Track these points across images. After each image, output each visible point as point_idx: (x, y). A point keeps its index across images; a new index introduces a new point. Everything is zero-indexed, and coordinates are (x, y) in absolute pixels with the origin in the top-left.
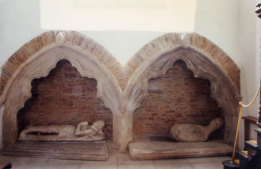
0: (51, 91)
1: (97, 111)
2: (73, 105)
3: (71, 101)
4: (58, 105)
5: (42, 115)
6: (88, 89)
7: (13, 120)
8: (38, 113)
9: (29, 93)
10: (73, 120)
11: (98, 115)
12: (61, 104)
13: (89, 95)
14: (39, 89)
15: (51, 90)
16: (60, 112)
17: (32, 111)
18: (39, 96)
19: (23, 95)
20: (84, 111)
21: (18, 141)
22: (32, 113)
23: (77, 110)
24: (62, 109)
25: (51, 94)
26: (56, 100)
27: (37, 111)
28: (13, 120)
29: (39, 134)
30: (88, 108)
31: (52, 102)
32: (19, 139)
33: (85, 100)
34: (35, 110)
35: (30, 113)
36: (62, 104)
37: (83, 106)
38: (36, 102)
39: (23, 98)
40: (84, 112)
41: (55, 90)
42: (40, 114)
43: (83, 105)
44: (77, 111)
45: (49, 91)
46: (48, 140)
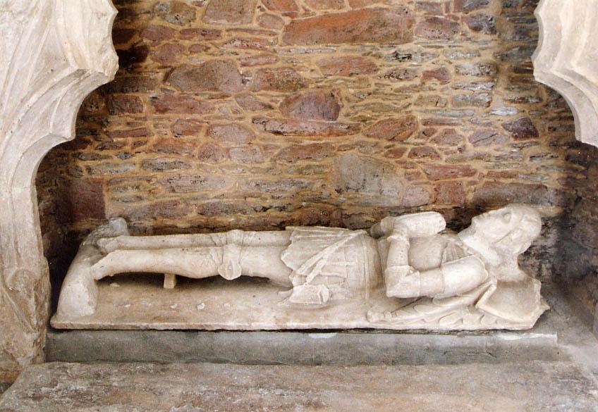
0: (218, 34)
1: (475, 144)
2: (343, 111)
3: (328, 91)
4: (256, 114)
5: (171, 166)
6: (433, 21)
7: (14, 216)
8: (143, 156)
9: (102, 51)
10: (339, 191)
11: (477, 165)
12: (270, 107)
13: (434, 55)
14: (145, 17)
15: (211, 25)
16: (266, 148)
17: (114, 146)
18: (149, 61)
19: (67, 64)
20: (398, 146)
21: (52, 329)
22: (111, 152)
23: (358, 137)
24: (278, 133)
25: (213, 49)
26: (243, 82)
27: (135, 145)
28: (14, 216)
29: (170, 283)
30: (422, 128)
31: (223, 97)
32: (56, 323)
33: (407, 84)
34: (130, 140)
35: (101, 158)
36: (282, 106)
37: (396, 116)
38: (130, 94)
39: (63, 82)
40: (398, 153)
41: (237, 25)
42: (159, 159)
43: (396, 110)
44: (360, 144)
45: (204, 33)
46: (231, 324)
